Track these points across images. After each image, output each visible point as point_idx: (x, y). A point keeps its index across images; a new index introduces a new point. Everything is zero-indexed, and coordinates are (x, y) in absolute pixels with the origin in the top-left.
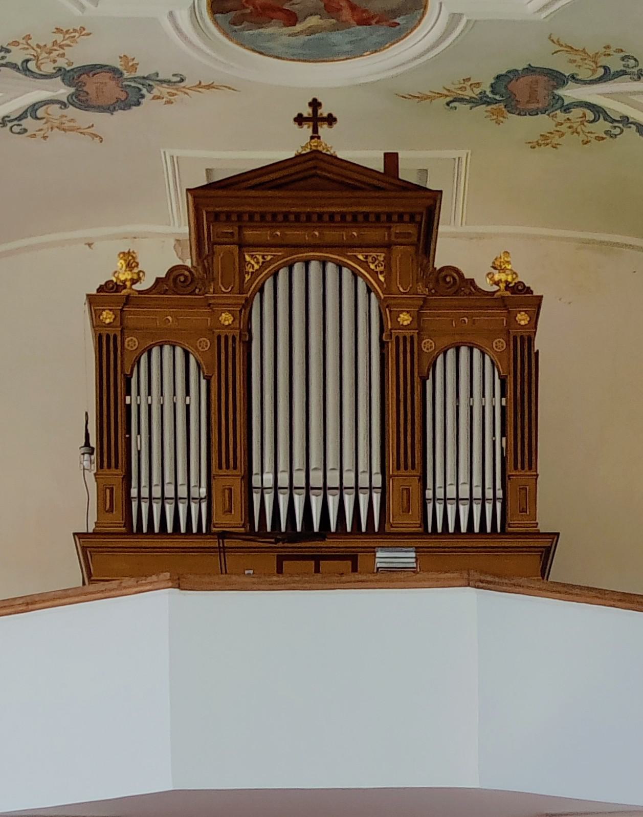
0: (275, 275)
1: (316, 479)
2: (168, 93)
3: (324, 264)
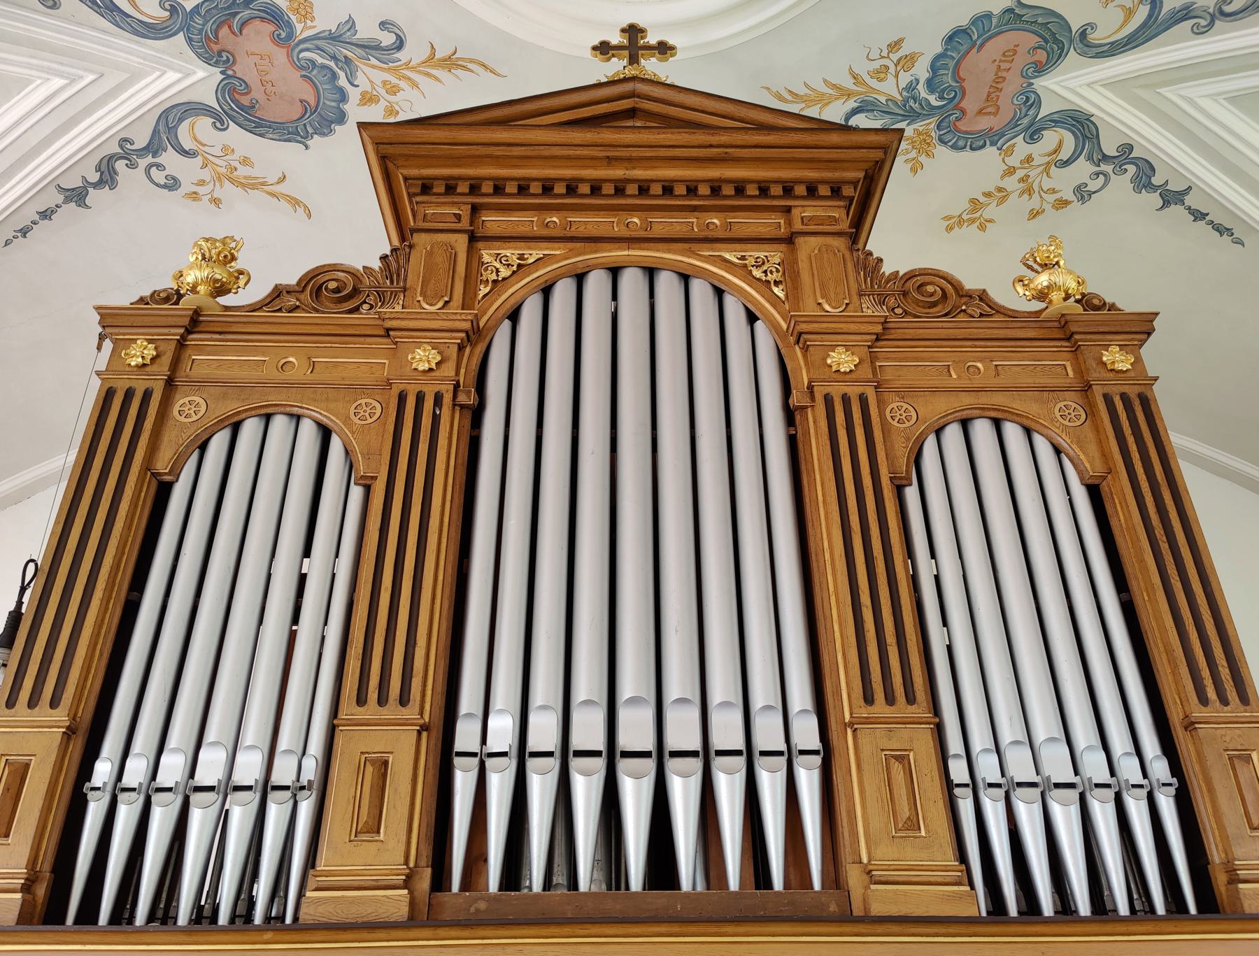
0: (547, 292)
1: (636, 730)
2: (384, 82)
3: (651, 273)
